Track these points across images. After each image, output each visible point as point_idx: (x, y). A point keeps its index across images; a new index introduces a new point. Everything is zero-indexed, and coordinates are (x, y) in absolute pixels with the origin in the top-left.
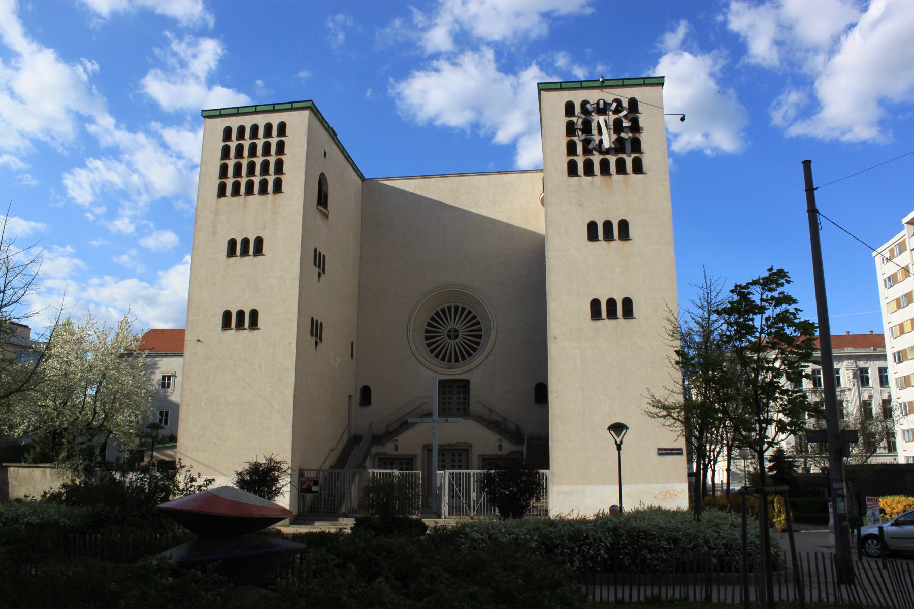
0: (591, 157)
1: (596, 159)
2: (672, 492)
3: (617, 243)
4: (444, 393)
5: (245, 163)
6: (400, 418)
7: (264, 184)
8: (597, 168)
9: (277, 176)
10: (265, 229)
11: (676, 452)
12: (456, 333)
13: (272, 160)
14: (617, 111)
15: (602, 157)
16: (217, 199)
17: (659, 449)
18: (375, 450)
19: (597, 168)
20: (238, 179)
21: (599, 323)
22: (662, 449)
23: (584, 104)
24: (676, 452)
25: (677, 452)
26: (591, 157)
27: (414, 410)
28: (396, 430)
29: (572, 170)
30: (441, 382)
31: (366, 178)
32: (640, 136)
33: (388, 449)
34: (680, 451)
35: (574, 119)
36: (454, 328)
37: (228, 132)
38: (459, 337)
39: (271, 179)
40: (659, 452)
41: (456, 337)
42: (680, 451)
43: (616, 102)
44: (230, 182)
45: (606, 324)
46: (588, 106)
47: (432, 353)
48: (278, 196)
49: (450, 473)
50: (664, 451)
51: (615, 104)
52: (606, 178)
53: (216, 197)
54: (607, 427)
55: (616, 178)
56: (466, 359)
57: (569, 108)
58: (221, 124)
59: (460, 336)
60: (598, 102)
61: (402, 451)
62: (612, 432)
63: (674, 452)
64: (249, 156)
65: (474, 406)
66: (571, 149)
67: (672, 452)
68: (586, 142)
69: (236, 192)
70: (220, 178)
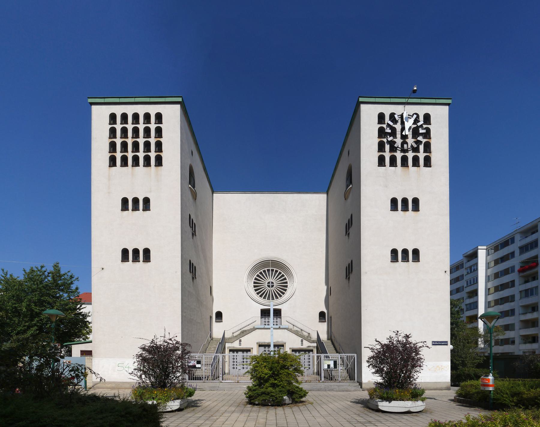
0: (395, 154)
1: (399, 155)
2: (440, 367)
3: (410, 213)
10: (150, 192)
11: (444, 343)
12: (273, 284)
13: (153, 140)
17: (433, 342)
21: (396, 264)
22: (435, 342)
23: (392, 116)
24: (444, 343)
25: (445, 343)
26: (395, 154)
29: (381, 161)
32: (430, 140)
34: (447, 343)
35: (385, 126)
37: (113, 117)
39: (153, 155)
40: (433, 343)
42: (447, 343)
44: (118, 155)
45: (400, 264)
46: (396, 116)
48: (160, 168)
50: (436, 343)
52: (405, 169)
55: (412, 169)
57: (381, 117)
63: (443, 343)
67: (441, 343)
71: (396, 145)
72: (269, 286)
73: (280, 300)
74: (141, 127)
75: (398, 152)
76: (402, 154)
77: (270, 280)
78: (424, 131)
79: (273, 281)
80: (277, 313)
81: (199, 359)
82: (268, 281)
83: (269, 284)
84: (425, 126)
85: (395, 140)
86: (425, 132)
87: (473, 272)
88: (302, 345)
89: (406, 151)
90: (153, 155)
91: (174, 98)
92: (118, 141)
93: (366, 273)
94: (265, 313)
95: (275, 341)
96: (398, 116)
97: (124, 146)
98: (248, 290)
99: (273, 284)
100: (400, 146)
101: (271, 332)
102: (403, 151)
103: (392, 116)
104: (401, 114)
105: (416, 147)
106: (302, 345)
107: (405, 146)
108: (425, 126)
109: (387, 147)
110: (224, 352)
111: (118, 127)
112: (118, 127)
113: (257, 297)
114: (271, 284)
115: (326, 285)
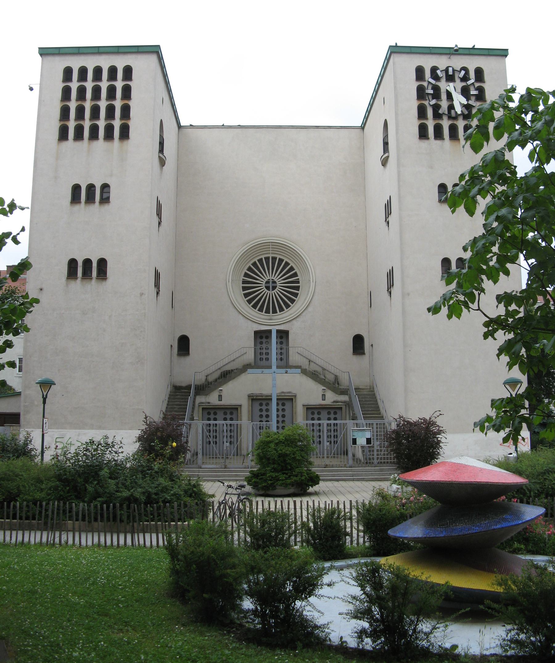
0: (440, 122)
1: (446, 124)
4: (261, 343)
5: (88, 105)
6: (219, 369)
7: (109, 129)
8: (101, 132)
9: (123, 122)
12: (274, 285)
13: (118, 104)
14: (465, 79)
15: (451, 122)
16: (58, 144)
18: (200, 399)
19: (101, 132)
20: (81, 122)
23: (434, 70)
26: (440, 122)
27: (234, 360)
28: (216, 380)
29: (423, 133)
30: (256, 333)
31: (181, 125)
33: (213, 399)
35: (425, 84)
36: (273, 280)
37: (68, 72)
38: (277, 288)
39: (117, 123)
41: (274, 288)
43: (464, 70)
44: (72, 124)
46: (438, 72)
47: (284, 310)
48: (125, 142)
49: (204, 424)
51: (463, 73)
53: (57, 140)
54: (503, 382)
56: (290, 306)
58: (61, 63)
59: (278, 287)
60: (447, 68)
61: (227, 401)
62: (507, 386)
64: (92, 99)
65: (294, 358)
66: (422, 112)
68: (436, 108)
69: (79, 135)
70: (61, 120)
71: (440, 112)
72: (268, 288)
73: (288, 314)
74: (104, 85)
75: (445, 118)
76: (451, 122)
77: (268, 277)
78: (476, 92)
79: (276, 280)
80: (281, 337)
81: (358, 428)
82: (266, 280)
83: (267, 285)
84: (477, 85)
85: (439, 103)
86: (477, 93)
87: (350, 398)
88: (324, 399)
89: (456, 118)
90: (117, 123)
91: (148, 51)
92: (73, 105)
93: (408, 294)
94: (261, 337)
95: (279, 391)
96: (441, 71)
97: (80, 111)
98: (233, 297)
99: (274, 285)
100: (446, 113)
101: (273, 380)
102: (450, 117)
103: (434, 70)
104: (444, 69)
105: (467, 114)
106: (324, 399)
107: (453, 111)
108: (477, 85)
109: (430, 112)
110: (239, 418)
111: (74, 85)
112: (74, 85)
113: (247, 309)
114: (271, 285)
115: (473, 48)
